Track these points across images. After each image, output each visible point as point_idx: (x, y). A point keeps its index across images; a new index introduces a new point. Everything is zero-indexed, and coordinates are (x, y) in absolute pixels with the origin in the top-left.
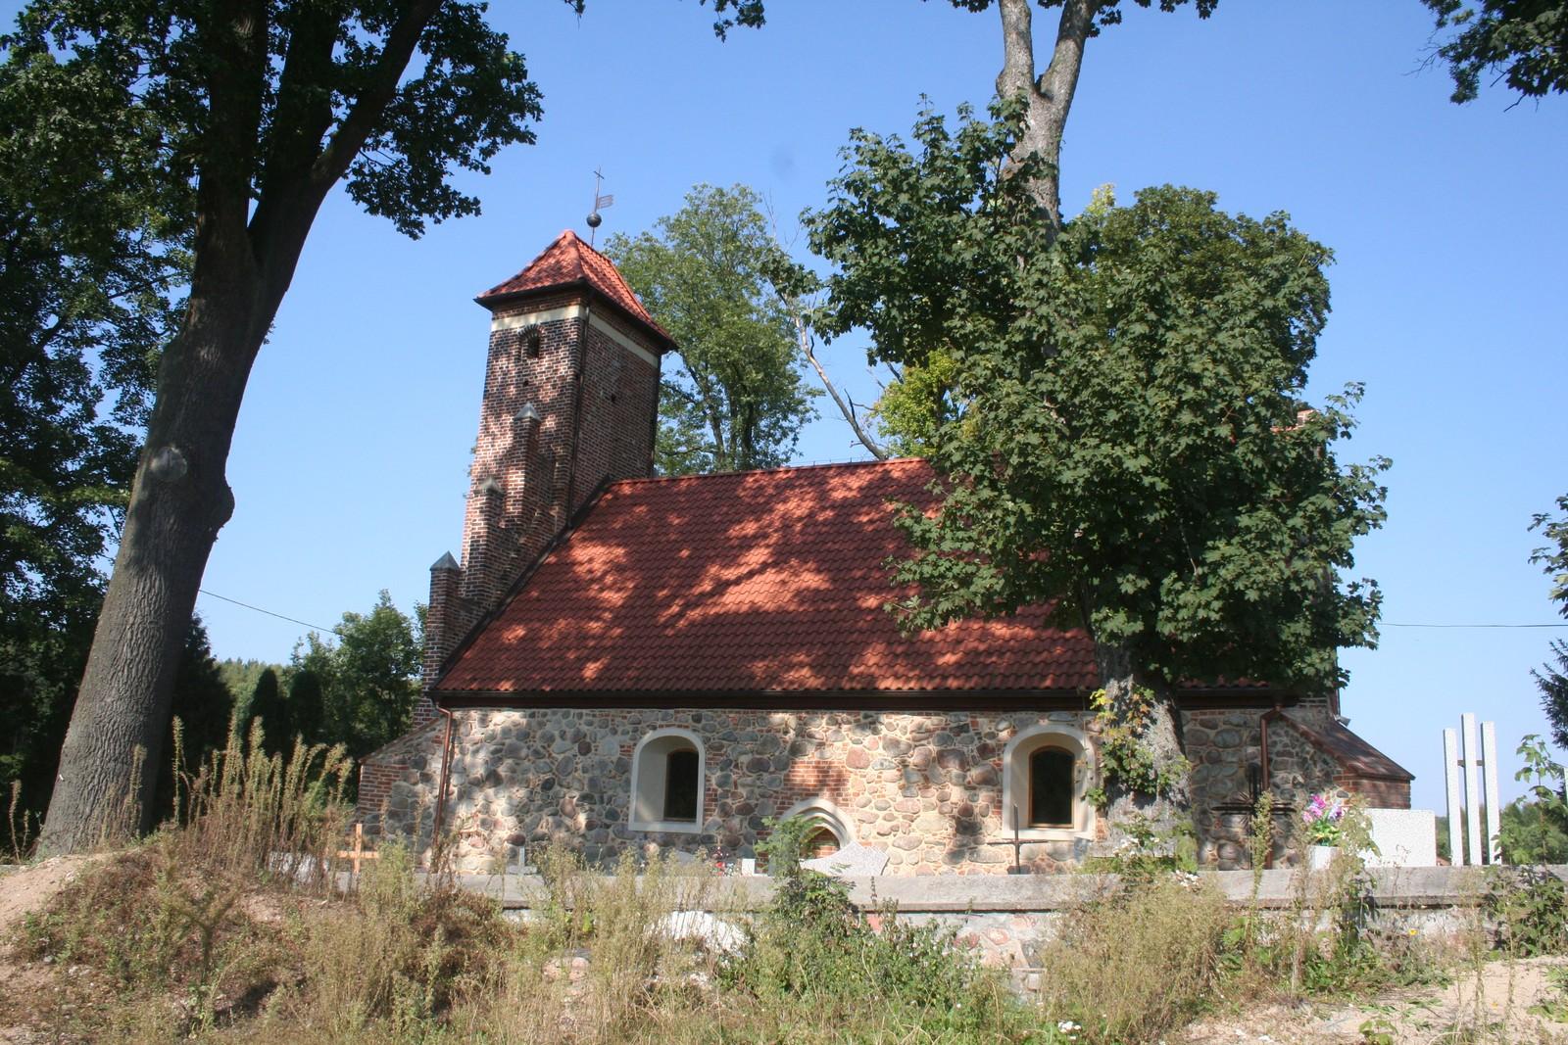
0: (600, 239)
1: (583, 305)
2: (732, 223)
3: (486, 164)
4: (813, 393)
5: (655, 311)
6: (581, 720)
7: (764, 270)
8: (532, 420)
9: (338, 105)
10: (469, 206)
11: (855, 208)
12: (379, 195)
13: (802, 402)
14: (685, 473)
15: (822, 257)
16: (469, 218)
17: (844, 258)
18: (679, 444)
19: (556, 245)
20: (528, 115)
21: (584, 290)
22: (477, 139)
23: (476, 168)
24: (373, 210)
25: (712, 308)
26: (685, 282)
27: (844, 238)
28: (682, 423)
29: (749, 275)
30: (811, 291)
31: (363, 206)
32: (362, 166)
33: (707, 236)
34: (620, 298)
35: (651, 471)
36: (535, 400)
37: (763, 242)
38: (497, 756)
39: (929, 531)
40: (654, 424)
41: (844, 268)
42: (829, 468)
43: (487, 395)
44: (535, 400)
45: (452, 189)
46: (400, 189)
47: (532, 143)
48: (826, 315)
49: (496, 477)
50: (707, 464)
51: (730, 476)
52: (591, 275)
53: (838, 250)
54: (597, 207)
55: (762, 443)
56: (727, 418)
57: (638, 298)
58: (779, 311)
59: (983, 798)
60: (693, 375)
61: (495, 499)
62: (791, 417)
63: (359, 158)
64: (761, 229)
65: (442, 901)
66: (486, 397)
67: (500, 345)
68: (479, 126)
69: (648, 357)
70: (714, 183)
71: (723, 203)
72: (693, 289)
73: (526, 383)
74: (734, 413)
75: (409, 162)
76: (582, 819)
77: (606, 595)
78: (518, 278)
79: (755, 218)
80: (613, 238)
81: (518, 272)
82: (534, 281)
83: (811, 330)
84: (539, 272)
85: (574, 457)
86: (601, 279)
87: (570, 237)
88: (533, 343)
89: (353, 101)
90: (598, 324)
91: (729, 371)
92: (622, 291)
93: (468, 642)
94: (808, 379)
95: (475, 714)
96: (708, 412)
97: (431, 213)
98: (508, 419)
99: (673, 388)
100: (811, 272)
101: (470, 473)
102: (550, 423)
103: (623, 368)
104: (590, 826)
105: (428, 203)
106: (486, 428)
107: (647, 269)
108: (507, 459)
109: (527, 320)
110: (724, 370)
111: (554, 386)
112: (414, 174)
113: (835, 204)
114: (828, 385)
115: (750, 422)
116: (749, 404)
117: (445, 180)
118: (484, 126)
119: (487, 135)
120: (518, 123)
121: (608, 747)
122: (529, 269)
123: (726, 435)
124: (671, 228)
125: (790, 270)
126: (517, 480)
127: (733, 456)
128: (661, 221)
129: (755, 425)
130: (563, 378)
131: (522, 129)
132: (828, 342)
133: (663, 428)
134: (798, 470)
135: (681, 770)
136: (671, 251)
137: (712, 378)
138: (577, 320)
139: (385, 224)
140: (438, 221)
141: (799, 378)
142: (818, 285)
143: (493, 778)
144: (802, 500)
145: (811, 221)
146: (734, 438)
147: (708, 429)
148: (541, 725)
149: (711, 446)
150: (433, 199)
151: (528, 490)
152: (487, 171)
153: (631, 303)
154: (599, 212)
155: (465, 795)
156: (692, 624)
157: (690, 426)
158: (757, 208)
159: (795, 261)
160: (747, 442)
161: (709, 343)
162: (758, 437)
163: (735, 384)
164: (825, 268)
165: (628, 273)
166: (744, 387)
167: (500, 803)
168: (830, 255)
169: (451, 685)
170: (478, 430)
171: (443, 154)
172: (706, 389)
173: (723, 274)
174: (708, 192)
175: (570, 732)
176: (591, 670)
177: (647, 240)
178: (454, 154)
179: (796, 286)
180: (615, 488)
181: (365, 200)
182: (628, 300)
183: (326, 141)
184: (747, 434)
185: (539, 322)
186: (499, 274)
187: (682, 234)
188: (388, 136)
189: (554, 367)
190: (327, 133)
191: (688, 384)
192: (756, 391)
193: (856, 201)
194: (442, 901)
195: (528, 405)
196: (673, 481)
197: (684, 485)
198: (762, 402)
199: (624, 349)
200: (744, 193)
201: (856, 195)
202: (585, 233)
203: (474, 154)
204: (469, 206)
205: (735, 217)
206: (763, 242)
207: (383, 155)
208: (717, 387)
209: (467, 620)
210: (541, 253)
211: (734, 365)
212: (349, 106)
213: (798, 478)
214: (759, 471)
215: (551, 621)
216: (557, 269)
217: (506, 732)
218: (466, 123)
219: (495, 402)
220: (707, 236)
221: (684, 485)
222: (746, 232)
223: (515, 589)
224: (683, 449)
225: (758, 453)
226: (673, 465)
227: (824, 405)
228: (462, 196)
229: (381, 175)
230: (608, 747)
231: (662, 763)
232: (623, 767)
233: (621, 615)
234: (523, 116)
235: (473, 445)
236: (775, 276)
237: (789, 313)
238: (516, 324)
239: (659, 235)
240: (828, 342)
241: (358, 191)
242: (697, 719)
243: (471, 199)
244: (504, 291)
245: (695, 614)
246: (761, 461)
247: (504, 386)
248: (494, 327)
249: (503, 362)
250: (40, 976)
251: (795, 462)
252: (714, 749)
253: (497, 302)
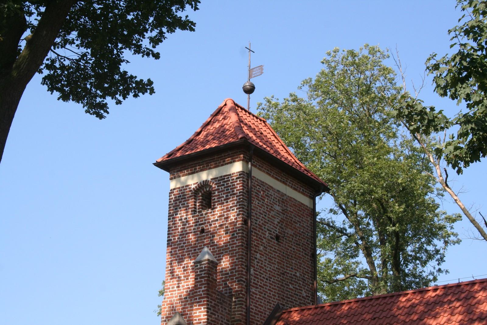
0: (253, 104)
1: (246, 161)
2: (365, 79)
3: (155, 51)
4: (452, 220)
5: (306, 160)
7: (400, 115)
8: (210, 262)
9: (31, 14)
10: (144, 87)
11: (475, 51)
12: (70, 85)
13: (441, 228)
14: (345, 298)
15: (447, 99)
16: (144, 97)
17: (468, 97)
18: (337, 273)
19: (219, 111)
20: (188, 7)
21: (243, 147)
22: (146, 31)
23: (148, 55)
24: (65, 97)
25: (356, 152)
26: (330, 133)
27: (467, 78)
28: (338, 254)
29: (385, 121)
30: (442, 128)
31: (57, 94)
32: (53, 61)
33: (346, 92)
34: (276, 151)
35: (315, 299)
36: (212, 244)
37: (394, 92)
39: (425, 272)
40: (314, 257)
41: (469, 106)
42: (473, 283)
43: (170, 243)
44: (212, 244)
45: (129, 74)
46: (87, 78)
47: (192, 30)
48: (456, 148)
49: (182, 314)
50: (364, 288)
51: (385, 298)
52: (251, 135)
53: (463, 91)
54: (250, 77)
55: (411, 266)
56: (376, 246)
57: (291, 150)
58: (414, 150)
60: (344, 212)
62: (435, 241)
63: (51, 55)
64: (391, 81)
66: (169, 245)
67: (178, 201)
68: (148, 19)
69: (304, 200)
70: (344, 48)
71: (355, 62)
72: (337, 137)
73: (203, 231)
74: (383, 242)
75: (92, 55)
78: (189, 142)
79: (385, 71)
80: (264, 102)
81: (189, 135)
82: (203, 144)
83: (443, 163)
84: (207, 136)
85: (248, 291)
86: (258, 137)
87: (230, 105)
88: (206, 196)
89: (43, 9)
90: (259, 175)
91: (374, 205)
92: (278, 146)
94: (446, 206)
96: (360, 242)
97: (113, 96)
98: (189, 262)
99: (328, 225)
100: (440, 112)
101: (160, 313)
102: (225, 263)
103: (284, 211)
105: (110, 87)
106: (172, 272)
107: (297, 125)
108: (191, 298)
109: (199, 177)
110: (370, 206)
111: (227, 232)
112: (97, 64)
113: (456, 49)
114: (464, 210)
115: (398, 249)
116: (396, 234)
117: (123, 67)
118: (151, 19)
119: (154, 27)
120: (179, 14)
122: (198, 134)
123: (378, 262)
124: (315, 88)
125: (422, 113)
127: (385, 279)
128: (306, 82)
129: (403, 250)
130: (233, 224)
131: (183, 19)
132: (459, 171)
133: (323, 260)
134: (445, 287)
136: (317, 108)
137: (361, 212)
138: (242, 173)
139: (76, 108)
140: (119, 102)
141: (438, 206)
142: (448, 124)
144: (452, 314)
145: (436, 67)
146: (384, 263)
147: (361, 258)
149: (365, 272)
150: (114, 83)
152: (157, 56)
153: (286, 155)
154: (253, 81)
157: (346, 256)
158: (385, 63)
159: (427, 105)
160: (397, 266)
161: (355, 183)
162: (407, 262)
163: (381, 215)
164: (453, 108)
165: (281, 130)
166: (390, 219)
168: (454, 97)
170: (164, 274)
171: (120, 45)
172: (356, 223)
173: (363, 123)
174: (339, 56)
177: (294, 101)
178: (128, 44)
179: (428, 126)
180: (285, 316)
181: (58, 90)
182: (283, 153)
183: (23, 44)
184: (396, 259)
185: (210, 177)
186: (174, 140)
187: (324, 92)
188: (74, 35)
189: (225, 216)
190: (23, 37)
191: (340, 220)
192: (400, 220)
193: (475, 45)
195: (206, 249)
196: (336, 305)
197: (345, 308)
198: (406, 231)
199: (283, 195)
200: (373, 51)
201: (475, 40)
202: (242, 100)
203: (145, 43)
204: (144, 87)
205: (368, 73)
206: (394, 92)
207: (70, 51)
208: (366, 221)
210: (207, 118)
211: (379, 201)
212: (39, 14)
213: (445, 295)
214: (410, 291)
218: (136, 18)
219: (178, 248)
220: (346, 92)
221: (345, 308)
222: (378, 84)
224: (341, 277)
225: (407, 275)
226: (333, 291)
227: (462, 228)
228: (138, 79)
229: (71, 67)
234: (183, 7)
235: (161, 288)
236: (410, 118)
237: (423, 151)
238: (192, 181)
239: (304, 95)
240: (459, 171)
241: (52, 83)
243: (145, 81)
244: (178, 155)
246: (411, 282)
247: (184, 234)
248: (173, 185)
249: (182, 214)
251: (443, 280)
253: (172, 164)
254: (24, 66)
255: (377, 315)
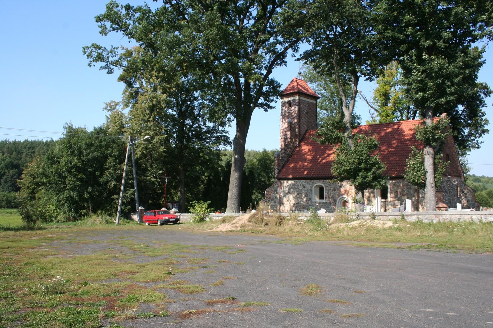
6: (303, 182)
19: (292, 81)
38: (289, 189)
43: (282, 115)
59: (372, 195)
61: (285, 139)
65: (280, 217)
76: (305, 200)
77: (308, 157)
82: (290, 90)
88: (290, 104)
93: (283, 167)
95: (285, 181)
103: (309, 106)
104: (306, 201)
121: (308, 187)
122: (287, 87)
126: (289, 134)
135: (321, 189)
143: (289, 193)
148: (297, 183)
151: (291, 136)
155: (285, 196)
156: (323, 163)
167: (291, 197)
169: (281, 176)
175: (302, 184)
176: (306, 173)
189: (295, 109)
194: (280, 217)
209: (282, 163)
215: (298, 163)
216: (293, 87)
217: (290, 185)
223: (290, 156)
230: (308, 187)
231: (318, 189)
232: (311, 190)
233: (311, 161)
238: (286, 100)
242: (323, 182)
245: (324, 161)
247: (285, 113)
250: (250, 223)
252: (326, 187)
254: (43, 249)
255: (441, 250)
